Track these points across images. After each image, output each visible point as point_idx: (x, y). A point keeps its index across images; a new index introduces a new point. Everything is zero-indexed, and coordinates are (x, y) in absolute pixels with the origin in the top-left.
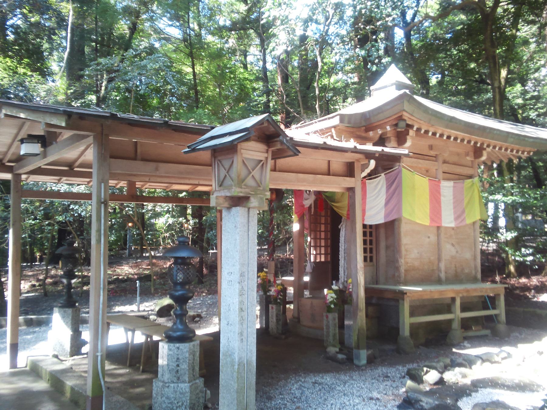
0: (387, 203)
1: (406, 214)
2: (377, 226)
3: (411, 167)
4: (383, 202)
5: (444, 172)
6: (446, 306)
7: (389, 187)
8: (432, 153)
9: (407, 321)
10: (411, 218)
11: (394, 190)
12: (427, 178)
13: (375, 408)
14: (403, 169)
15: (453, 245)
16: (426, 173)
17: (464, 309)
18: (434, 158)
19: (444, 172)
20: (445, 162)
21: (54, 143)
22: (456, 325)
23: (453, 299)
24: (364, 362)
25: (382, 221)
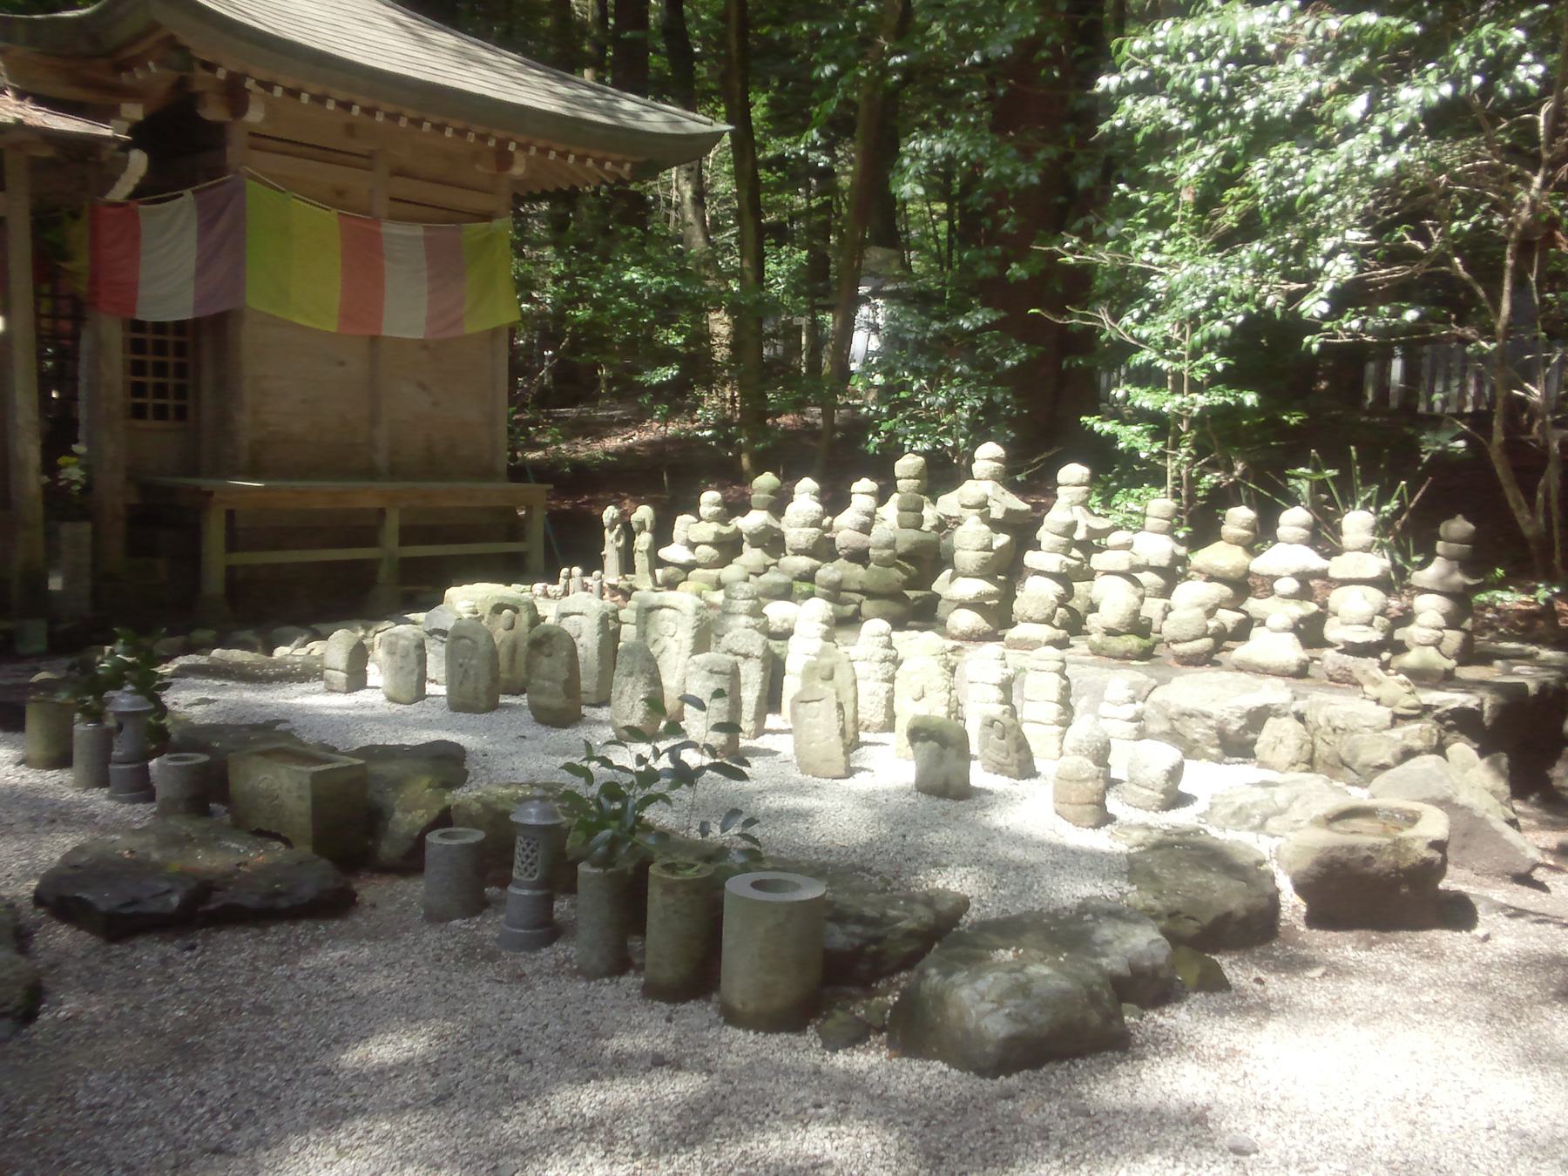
0: (201, 271)
1: (256, 300)
2: (180, 327)
3: (272, 177)
4: (190, 265)
5: (392, 199)
6: (363, 531)
7: (206, 225)
8: (356, 146)
9: (216, 558)
10: (273, 312)
11: (224, 238)
12: (334, 211)
13: (903, 1171)
14: (250, 183)
15: (423, 387)
16: (336, 198)
17: (409, 535)
18: (364, 162)
19: (392, 199)
20: (400, 172)
21: (1550, 694)
22: (384, 573)
23: (382, 513)
24: (41, 646)
25: (187, 315)
